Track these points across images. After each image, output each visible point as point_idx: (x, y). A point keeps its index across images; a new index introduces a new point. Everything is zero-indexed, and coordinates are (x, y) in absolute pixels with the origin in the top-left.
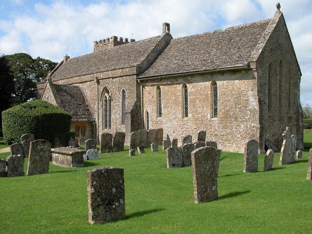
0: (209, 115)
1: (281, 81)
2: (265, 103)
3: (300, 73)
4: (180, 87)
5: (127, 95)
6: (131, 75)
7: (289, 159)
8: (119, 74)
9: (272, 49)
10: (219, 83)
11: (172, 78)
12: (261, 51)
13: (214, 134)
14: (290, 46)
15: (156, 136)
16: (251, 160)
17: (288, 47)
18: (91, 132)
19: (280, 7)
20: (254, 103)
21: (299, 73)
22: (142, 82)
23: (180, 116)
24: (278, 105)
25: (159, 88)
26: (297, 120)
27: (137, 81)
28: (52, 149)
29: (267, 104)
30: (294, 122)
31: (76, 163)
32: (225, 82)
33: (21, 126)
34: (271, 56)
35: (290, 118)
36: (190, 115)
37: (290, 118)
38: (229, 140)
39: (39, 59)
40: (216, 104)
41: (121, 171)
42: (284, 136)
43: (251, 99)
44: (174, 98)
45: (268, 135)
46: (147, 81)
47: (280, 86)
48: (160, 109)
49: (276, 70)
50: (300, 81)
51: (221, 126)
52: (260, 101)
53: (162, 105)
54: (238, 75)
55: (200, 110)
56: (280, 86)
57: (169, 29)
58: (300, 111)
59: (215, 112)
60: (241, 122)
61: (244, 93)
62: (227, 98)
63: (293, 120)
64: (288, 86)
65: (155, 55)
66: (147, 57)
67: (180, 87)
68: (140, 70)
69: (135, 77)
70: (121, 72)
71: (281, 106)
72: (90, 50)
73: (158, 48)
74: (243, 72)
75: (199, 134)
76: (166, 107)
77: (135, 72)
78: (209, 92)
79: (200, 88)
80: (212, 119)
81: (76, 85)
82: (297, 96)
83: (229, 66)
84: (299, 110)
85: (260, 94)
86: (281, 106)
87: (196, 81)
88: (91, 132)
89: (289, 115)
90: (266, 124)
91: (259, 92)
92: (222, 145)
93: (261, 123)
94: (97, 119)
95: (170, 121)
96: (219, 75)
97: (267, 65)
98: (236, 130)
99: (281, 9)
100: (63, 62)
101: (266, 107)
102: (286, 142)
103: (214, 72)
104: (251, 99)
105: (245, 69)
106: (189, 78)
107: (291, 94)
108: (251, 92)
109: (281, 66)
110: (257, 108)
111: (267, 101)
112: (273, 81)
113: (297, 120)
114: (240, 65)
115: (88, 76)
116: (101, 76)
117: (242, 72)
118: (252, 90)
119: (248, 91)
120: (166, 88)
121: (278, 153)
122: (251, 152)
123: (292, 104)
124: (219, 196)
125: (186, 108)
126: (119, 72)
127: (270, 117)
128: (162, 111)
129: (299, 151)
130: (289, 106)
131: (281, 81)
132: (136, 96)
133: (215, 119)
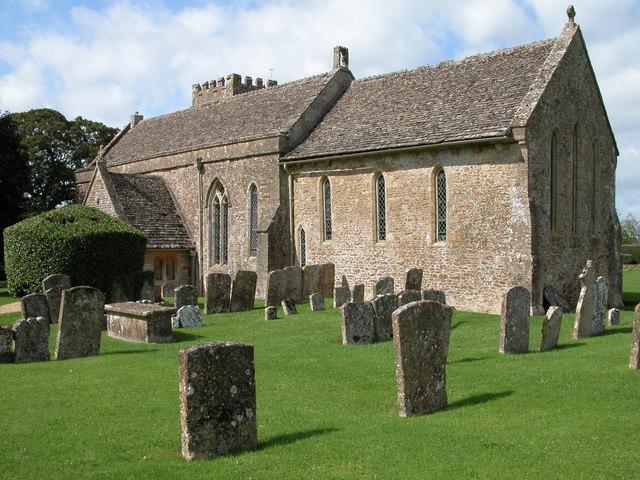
0: (428, 237)
1: (576, 167)
2: (544, 212)
3: (616, 149)
4: (368, 179)
5: (260, 194)
6: (269, 154)
7: (592, 326)
8: (243, 153)
9: (557, 101)
10: (449, 170)
11: (352, 161)
12: (535, 104)
13: (438, 275)
14: (595, 95)
15: (321, 278)
16: (514, 329)
17: (591, 96)
18: (186, 271)
19: (574, 14)
20: (521, 212)
21: (614, 150)
22: (292, 169)
23: (370, 238)
24: (570, 216)
25: (325, 181)
26: (610, 247)
27: (281, 167)
28: (107, 306)
29: (549, 213)
30: (602, 249)
31: (155, 334)
32: (461, 168)
33: (43, 259)
34: (556, 114)
35: (595, 242)
36: (389, 236)
37: (595, 242)
38: (470, 287)
39: (80, 121)
40: (442, 212)
41: (248, 351)
42: (583, 279)
43: (516, 203)
44: (358, 200)
45: (550, 276)
46: (302, 165)
47: (575, 176)
48: (329, 223)
49: (567, 144)
50: (615, 167)
51: (454, 258)
52: (533, 208)
53: (333, 216)
54: (489, 154)
55: (409, 226)
56: (575, 176)
57: (346, 60)
58: (616, 227)
59: (441, 230)
60: (494, 251)
61: (501, 190)
62: (465, 202)
63: (602, 247)
64: (590, 177)
65: (318, 112)
66: (302, 117)
67: (368, 179)
68: (288, 144)
69: (277, 157)
70: (249, 148)
71: (575, 217)
72: (186, 102)
73: (325, 98)
74: (499, 148)
75: (409, 274)
76: (340, 219)
77: (277, 148)
78: (429, 189)
79: (410, 182)
80: (436, 244)
81: (155, 174)
82: (609, 198)
83: (470, 135)
84: (613, 226)
85: (534, 193)
86: (575, 217)
87: (402, 167)
88: (186, 271)
89: (593, 236)
90: (546, 255)
91: (531, 188)
92: (455, 297)
93: (535, 252)
94: (198, 244)
95: (349, 248)
96: (449, 155)
97: (548, 133)
98: (483, 266)
99: (577, 19)
100: (128, 127)
101: (545, 220)
102: (586, 292)
103: (440, 147)
104: (516, 203)
105: (502, 143)
106: (388, 160)
107: (597, 193)
108: (514, 189)
109: (576, 135)
110: (527, 221)
111: (547, 207)
112: (560, 167)
113: (610, 247)
114: (493, 134)
115: (181, 156)
116: (207, 155)
117: (496, 147)
118: (517, 185)
119: (509, 186)
120: (341, 180)
121: (571, 314)
122: (514, 311)
123: (599, 213)
124: (449, 403)
125: (382, 222)
126: (244, 148)
127: (553, 239)
128: (333, 227)
129: (613, 309)
130: (593, 217)
131: (576, 167)
132: (278, 197)
133: (441, 244)
